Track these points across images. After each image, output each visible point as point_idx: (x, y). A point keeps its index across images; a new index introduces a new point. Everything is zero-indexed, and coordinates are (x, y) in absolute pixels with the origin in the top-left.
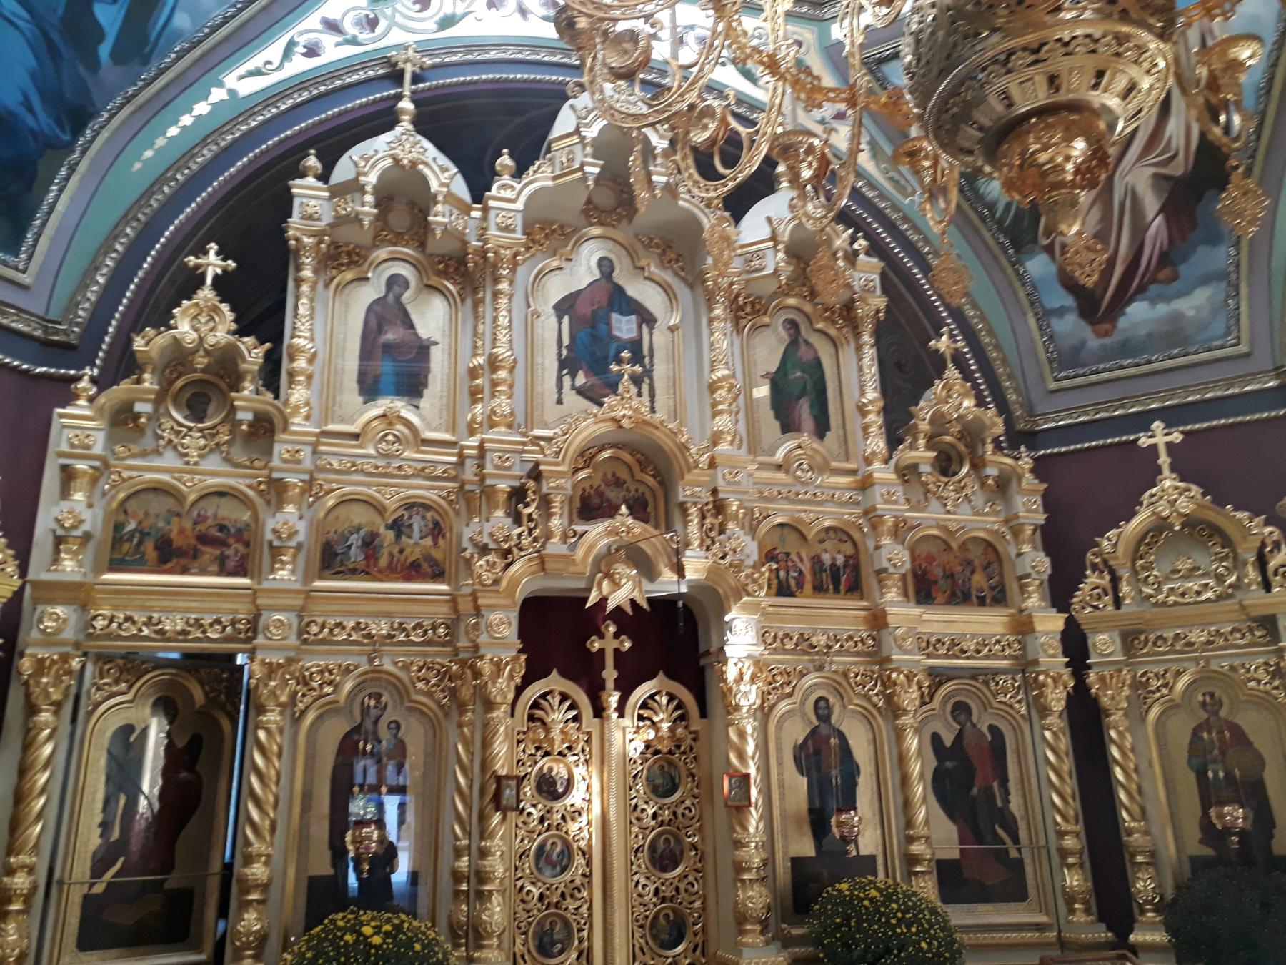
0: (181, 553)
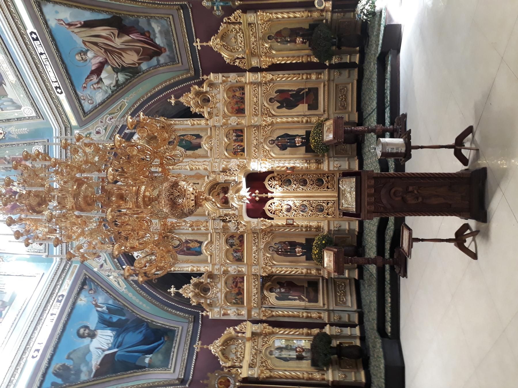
0: (239, 291)
